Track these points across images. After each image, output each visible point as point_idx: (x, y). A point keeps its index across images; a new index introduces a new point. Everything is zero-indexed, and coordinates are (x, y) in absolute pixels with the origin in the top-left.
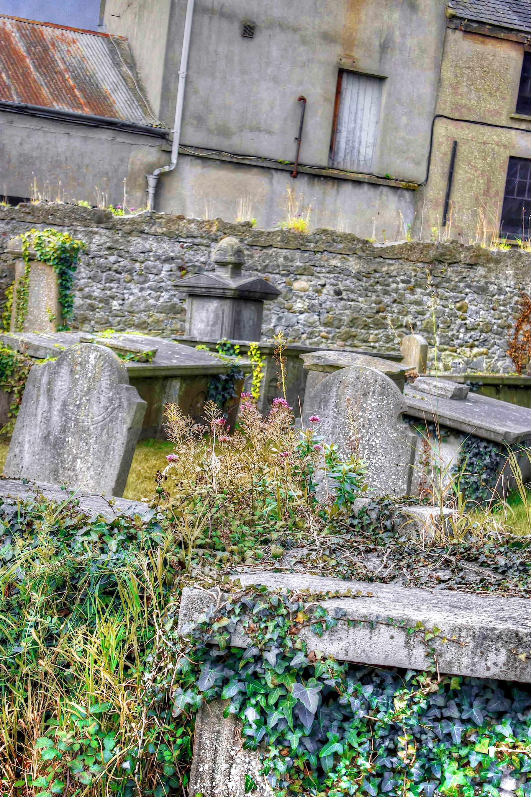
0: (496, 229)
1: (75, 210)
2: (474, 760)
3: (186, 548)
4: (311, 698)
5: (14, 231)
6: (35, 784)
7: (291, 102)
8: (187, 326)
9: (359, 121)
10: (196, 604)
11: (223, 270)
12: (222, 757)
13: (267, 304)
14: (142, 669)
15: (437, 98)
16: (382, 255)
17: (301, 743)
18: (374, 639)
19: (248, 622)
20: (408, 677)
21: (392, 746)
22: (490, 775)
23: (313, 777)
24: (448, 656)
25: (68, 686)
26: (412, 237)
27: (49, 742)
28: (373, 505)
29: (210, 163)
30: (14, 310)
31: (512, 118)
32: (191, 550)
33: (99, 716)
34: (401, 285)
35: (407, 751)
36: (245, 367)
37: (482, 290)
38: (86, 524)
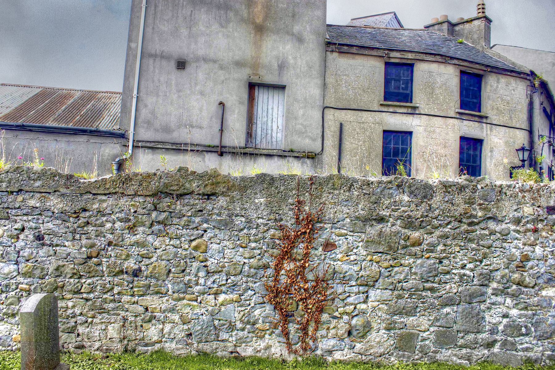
7: (214, 108)
9: (270, 116)
31: (381, 105)
34: (118, 225)
37: (226, 224)
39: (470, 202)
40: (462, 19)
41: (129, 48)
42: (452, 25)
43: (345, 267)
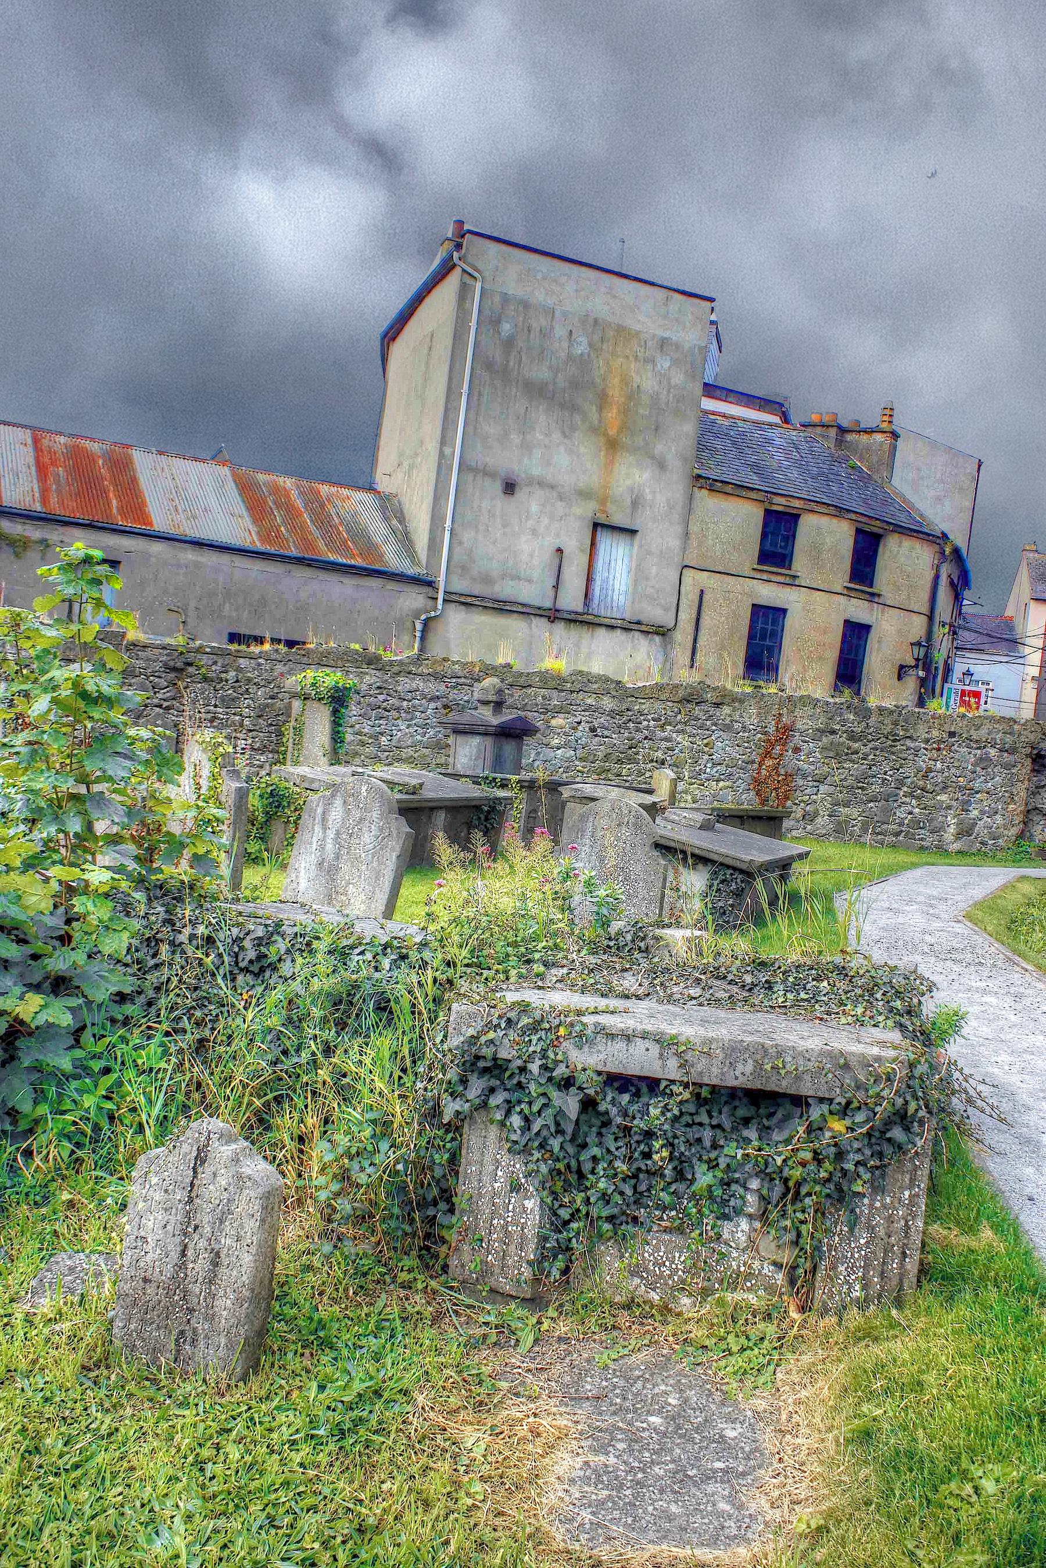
0: (741, 669)
1: (348, 652)
2: (723, 1162)
3: (455, 966)
4: (571, 1104)
5: (290, 672)
6: (315, 1183)
8: (451, 760)
10: (464, 1019)
11: (485, 707)
12: (488, 1158)
15: (684, 549)
16: (635, 694)
17: (562, 1148)
18: (631, 1051)
19: (512, 1035)
20: (662, 1087)
21: (647, 1150)
22: (737, 1175)
23: (573, 1178)
24: (699, 1067)
25: (346, 1094)
26: (662, 677)
27: (328, 1145)
28: (629, 928)
29: (473, 608)
30: (290, 744)
32: (459, 968)
33: (374, 1122)
34: (652, 723)
35: (660, 1155)
36: (505, 798)
37: (727, 728)
38: (360, 944)
39: (895, 724)
40: (858, 423)
41: (441, 454)
42: (842, 430)
43: (806, 766)
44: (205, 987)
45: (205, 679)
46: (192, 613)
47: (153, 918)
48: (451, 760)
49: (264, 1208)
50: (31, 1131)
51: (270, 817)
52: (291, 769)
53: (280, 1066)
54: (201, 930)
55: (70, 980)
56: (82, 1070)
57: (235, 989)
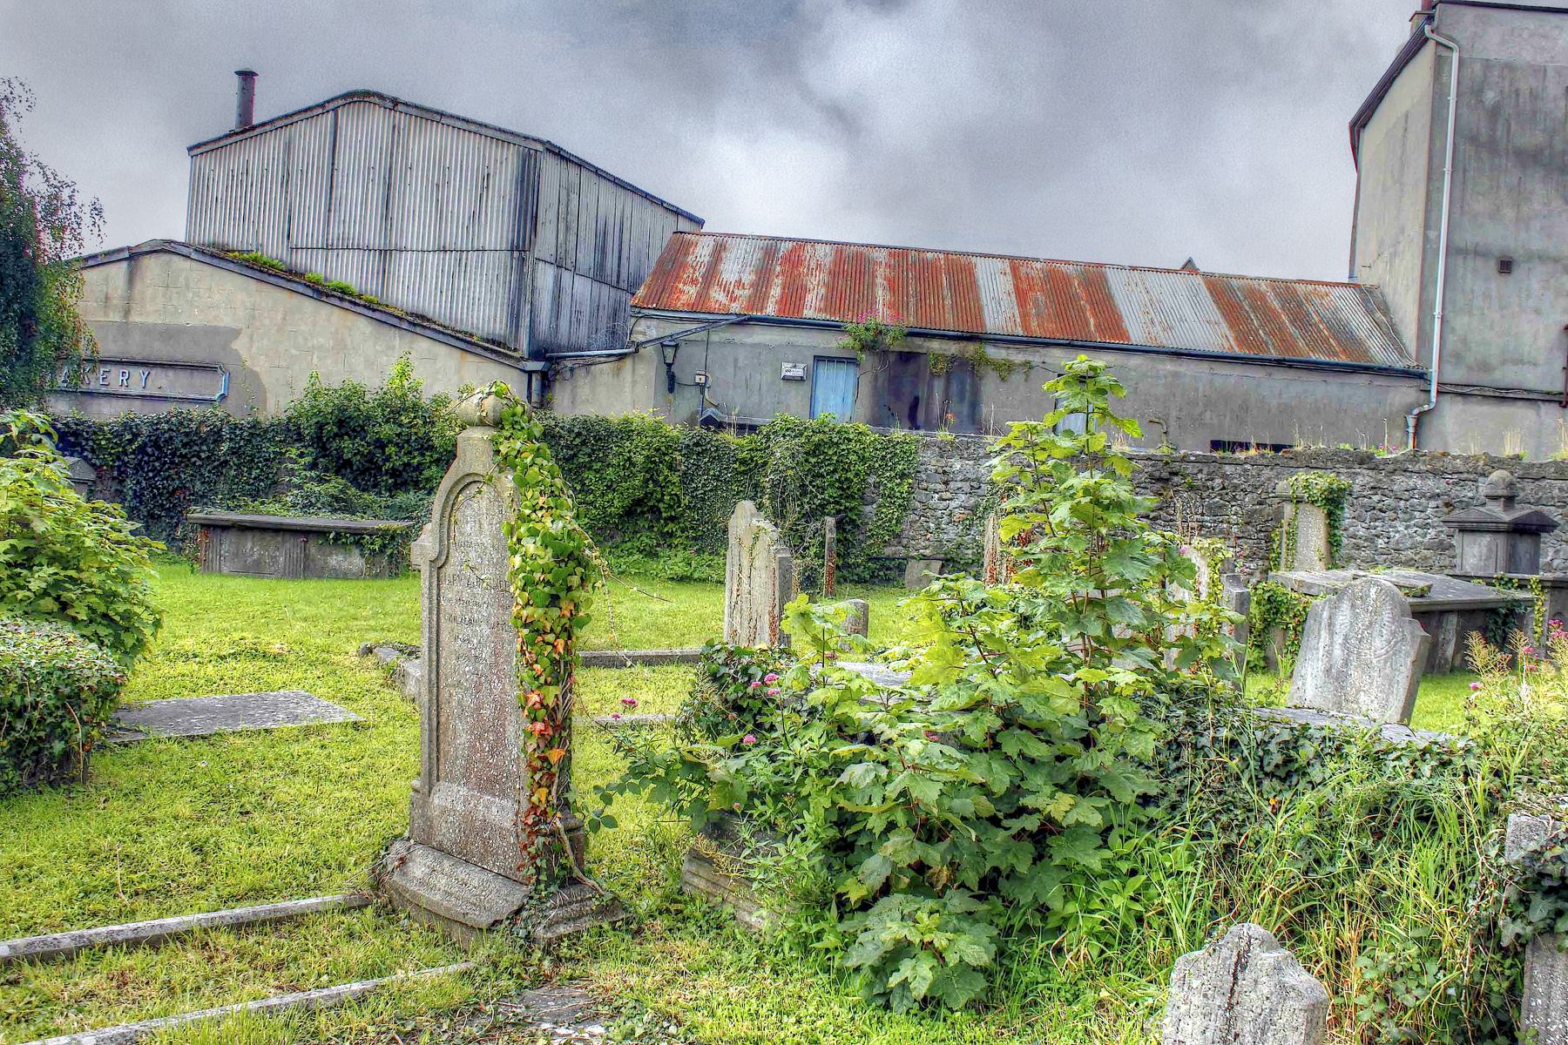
8: (1457, 561)
13: (1545, 537)
14: (1462, 895)
27: (1368, 962)
29: (1474, 399)
33: (1419, 940)
41: (1426, 239)
44: (1230, 791)
45: (1191, 488)
46: (1172, 422)
47: (1174, 721)
48: (1457, 561)
49: (1309, 1022)
50: (1059, 930)
51: (1268, 625)
52: (1289, 575)
53: (1312, 875)
54: (1224, 733)
55: (1096, 781)
56: (1110, 871)
57: (1260, 793)
